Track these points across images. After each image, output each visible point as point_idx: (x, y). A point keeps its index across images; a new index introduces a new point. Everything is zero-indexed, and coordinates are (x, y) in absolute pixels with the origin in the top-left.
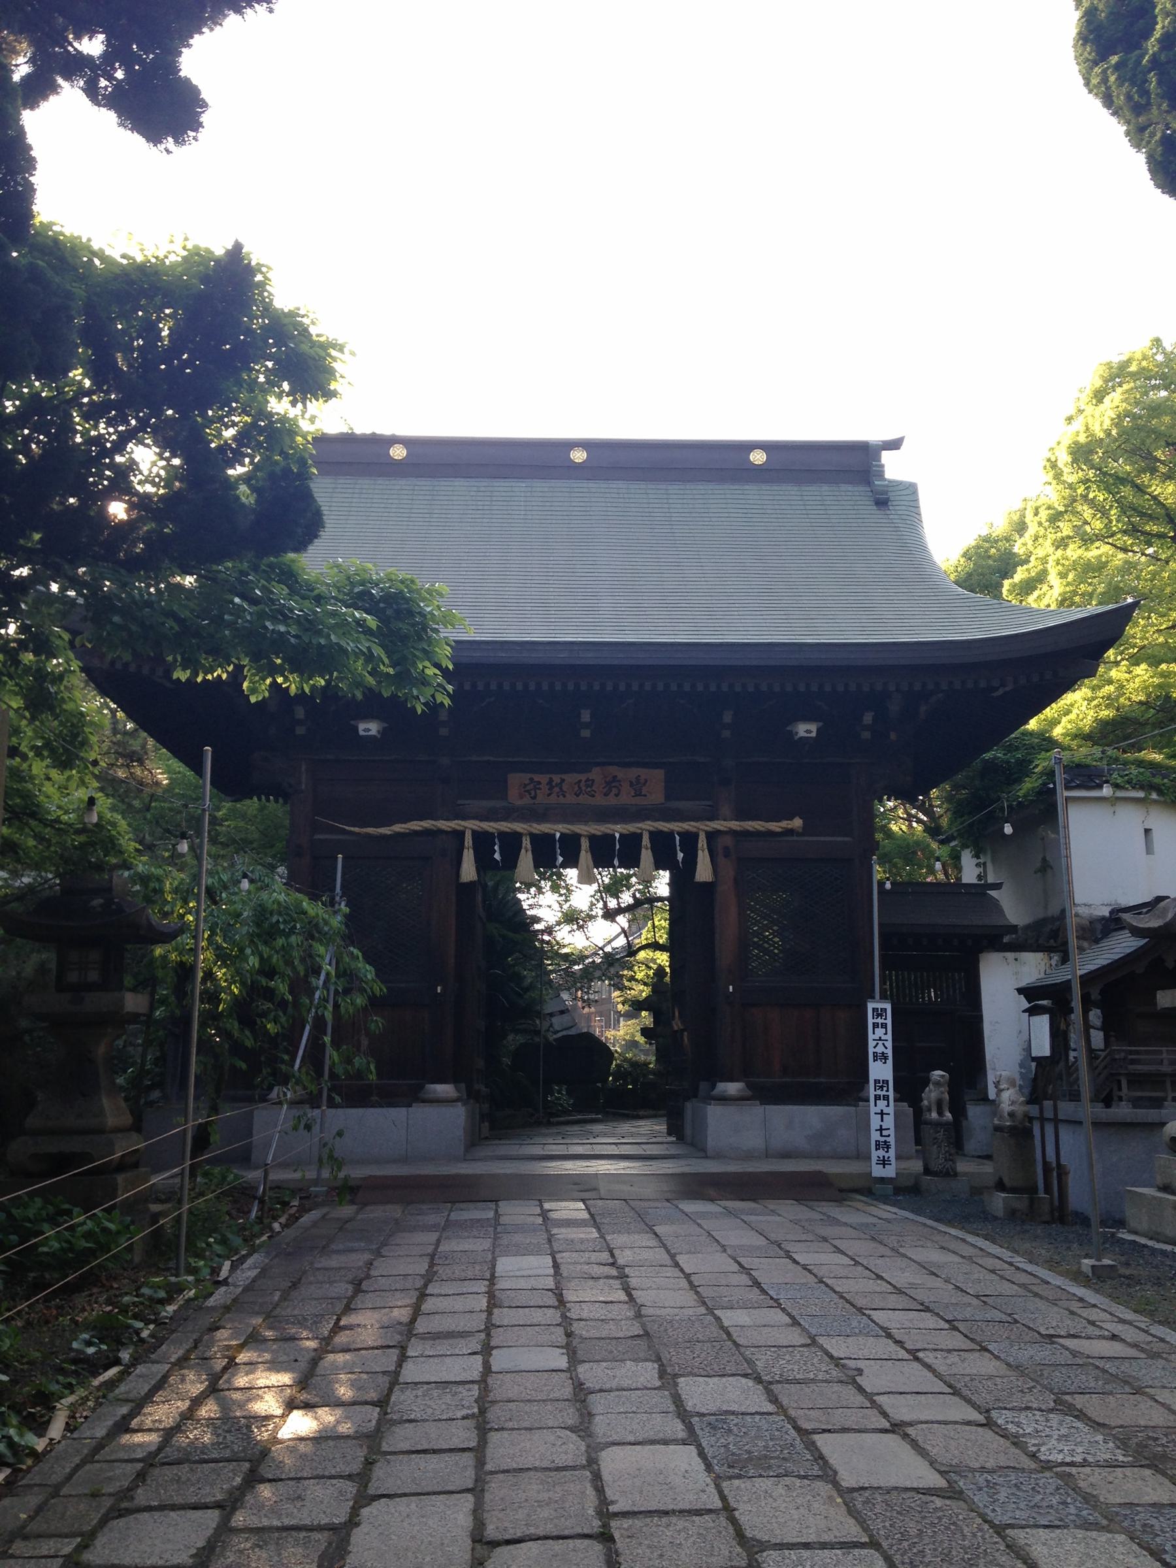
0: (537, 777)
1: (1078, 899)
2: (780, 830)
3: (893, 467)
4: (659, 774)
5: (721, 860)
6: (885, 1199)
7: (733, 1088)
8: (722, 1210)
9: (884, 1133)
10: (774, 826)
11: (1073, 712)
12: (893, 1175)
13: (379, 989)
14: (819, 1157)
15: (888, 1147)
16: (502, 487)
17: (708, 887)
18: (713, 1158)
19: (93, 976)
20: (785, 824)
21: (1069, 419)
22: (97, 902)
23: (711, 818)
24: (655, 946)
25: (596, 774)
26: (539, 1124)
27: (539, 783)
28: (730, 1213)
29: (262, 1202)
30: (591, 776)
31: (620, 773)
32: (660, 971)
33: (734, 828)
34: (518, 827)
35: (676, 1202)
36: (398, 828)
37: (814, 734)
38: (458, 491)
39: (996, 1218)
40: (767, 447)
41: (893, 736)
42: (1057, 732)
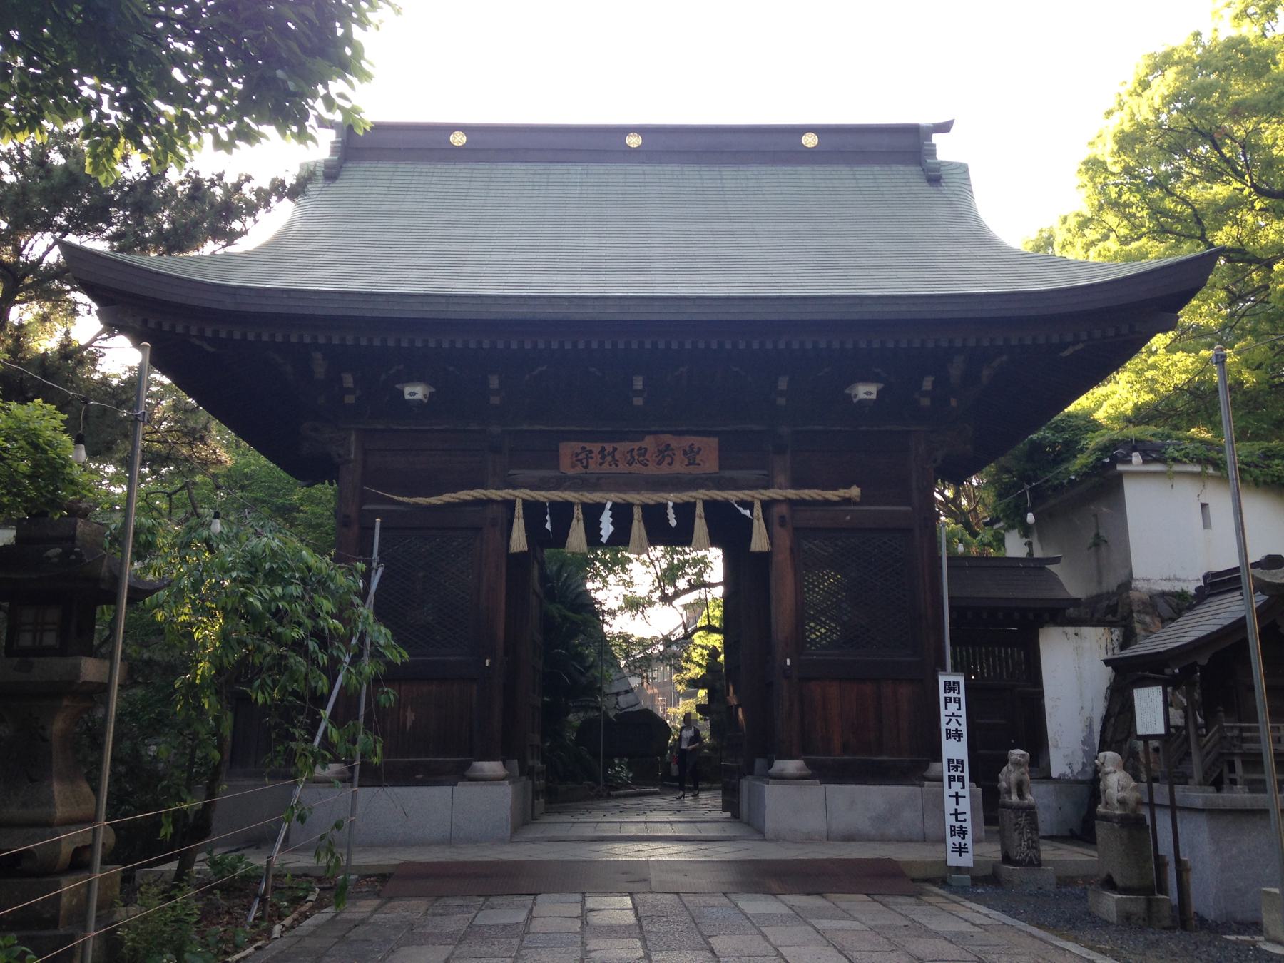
0: (588, 446)
1: (1138, 572)
2: (836, 499)
3: (945, 149)
4: (714, 442)
5: (777, 529)
6: (962, 891)
7: (792, 766)
8: (785, 910)
9: (960, 817)
10: (831, 495)
11: (1112, 399)
12: (971, 864)
13: (399, 656)
14: (884, 839)
15: (964, 833)
16: (558, 170)
17: (764, 557)
18: (771, 840)
19: (50, 639)
20: (842, 493)
21: (1109, 113)
22: (55, 551)
23: (766, 488)
24: (710, 629)
25: (648, 442)
26: (599, 797)
27: (591, 452)
28: (799, 916)
29: (263, 900)
30: (643, 444)
31: (673, 441)
32: (714, 653)
33: (790, 496)
34: (570, 496)
35: (734, 897)
36: (448, 497)
37: (874, 397)
38: (517, 177)
39: (1107, 924)
40: (820, 130)
41: (953, 402)
42: (1099, 415)
